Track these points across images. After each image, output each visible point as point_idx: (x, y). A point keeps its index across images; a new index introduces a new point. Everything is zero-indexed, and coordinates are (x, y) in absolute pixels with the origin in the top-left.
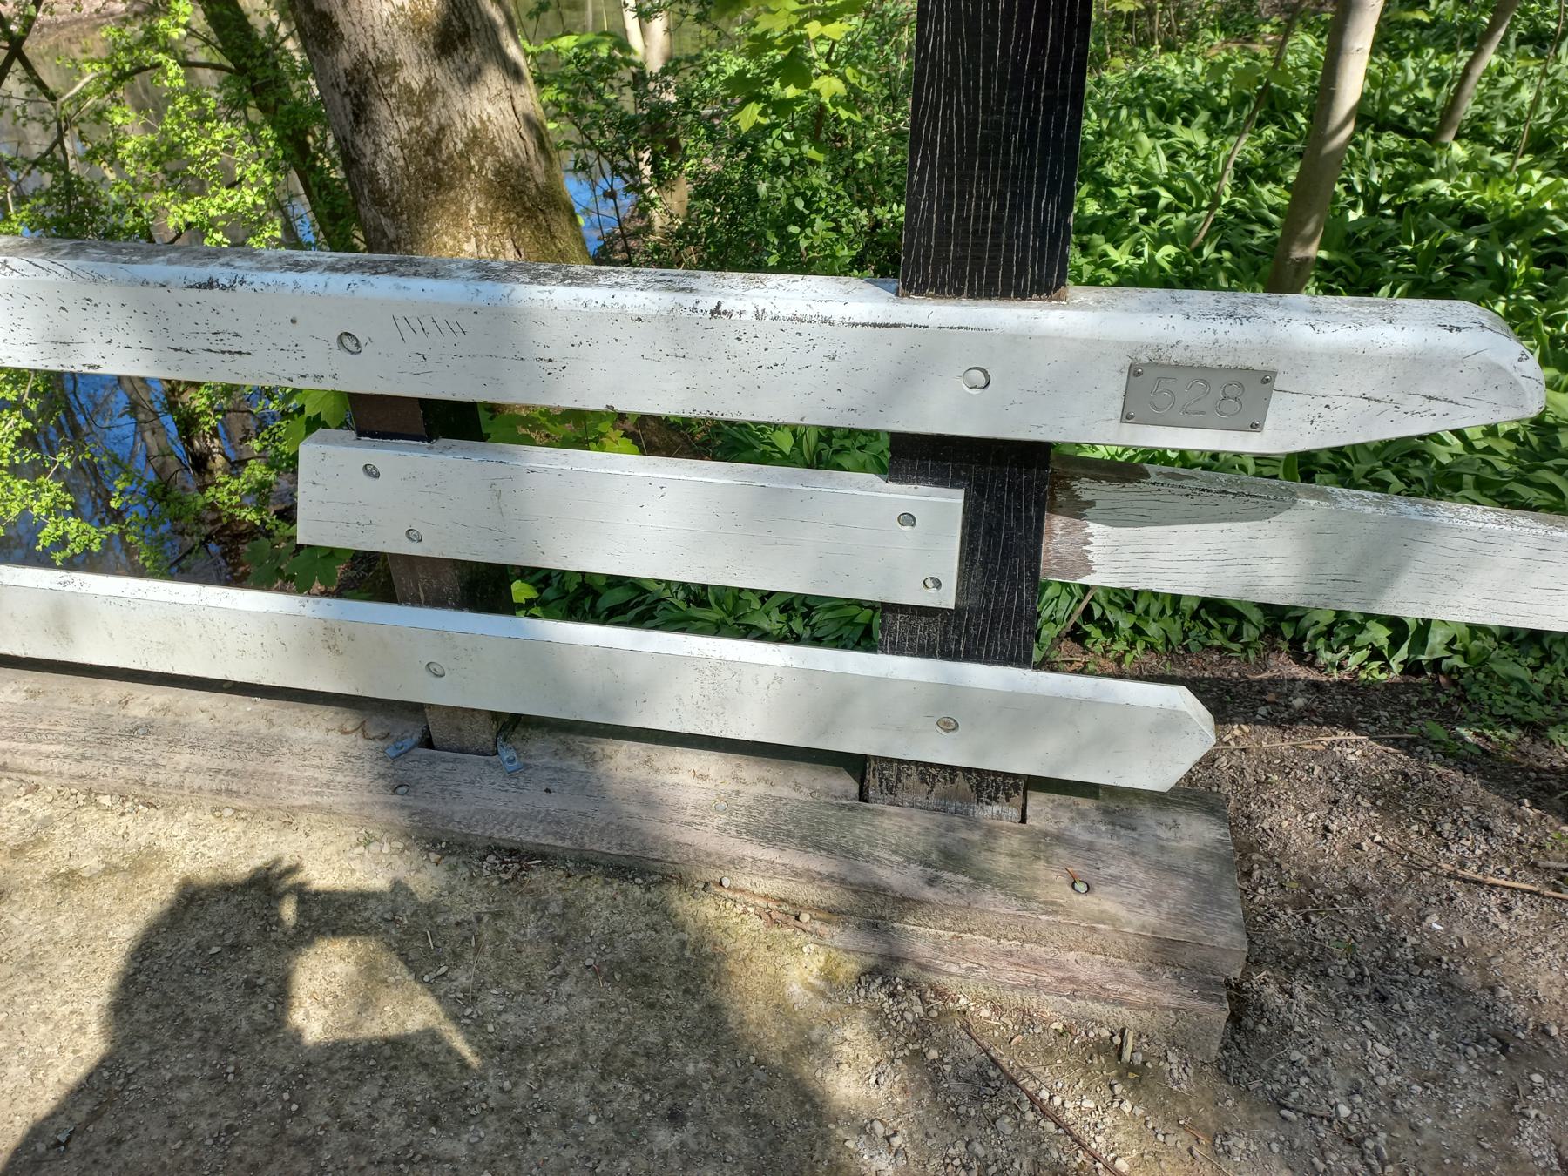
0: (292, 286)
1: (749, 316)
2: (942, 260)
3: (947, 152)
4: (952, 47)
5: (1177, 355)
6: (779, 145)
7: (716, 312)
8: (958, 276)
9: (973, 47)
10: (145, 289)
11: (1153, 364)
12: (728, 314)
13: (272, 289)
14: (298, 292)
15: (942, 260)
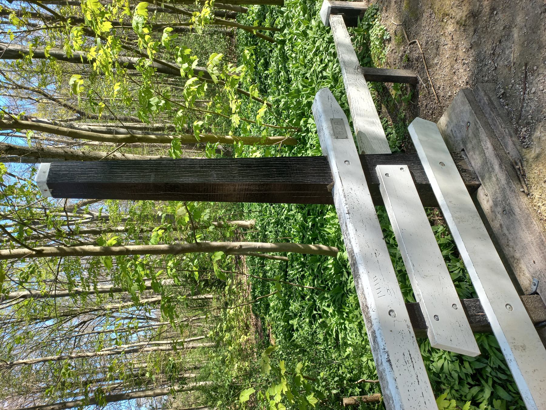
0: (380, 330)
1: (347, 206)
2: (325, 176)
3: (302, 177)
4: (283, 177)
5: (332, 132)
6: (320, 387)
7: (349, 213)
8: (327, 173)
9: (282, 174)
10: (399, 387)
11: (334, 135)
12: (348, 211)
13: (383, 337)
14: (381, 328)
15: (325, 176)
